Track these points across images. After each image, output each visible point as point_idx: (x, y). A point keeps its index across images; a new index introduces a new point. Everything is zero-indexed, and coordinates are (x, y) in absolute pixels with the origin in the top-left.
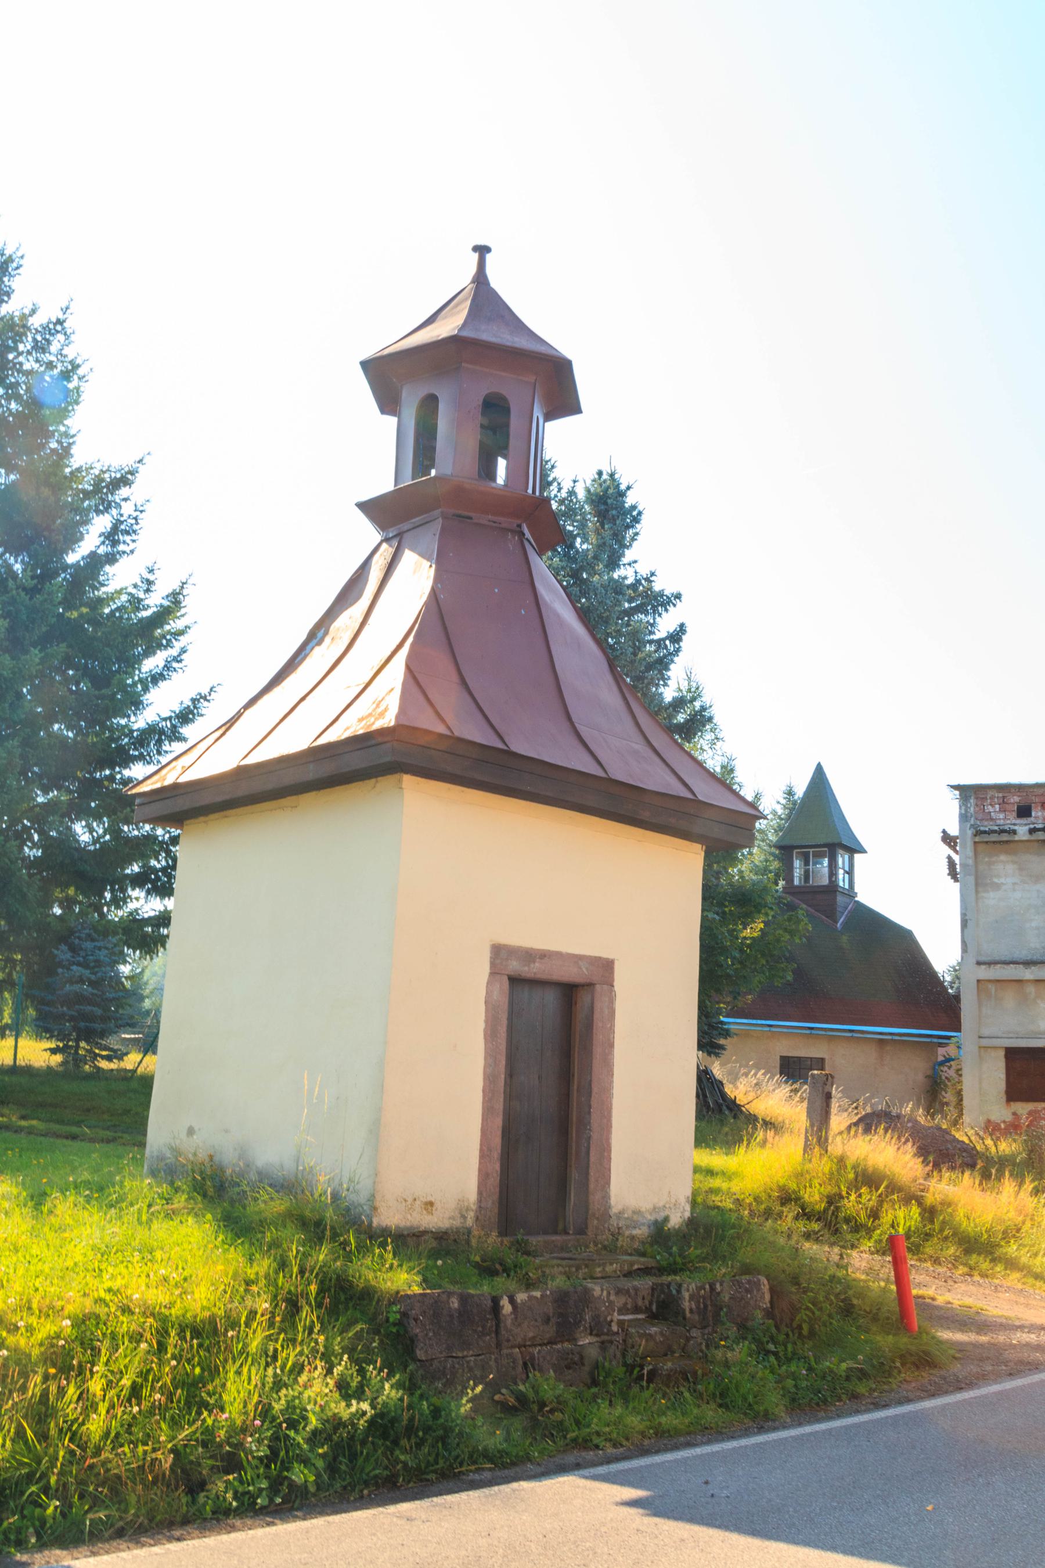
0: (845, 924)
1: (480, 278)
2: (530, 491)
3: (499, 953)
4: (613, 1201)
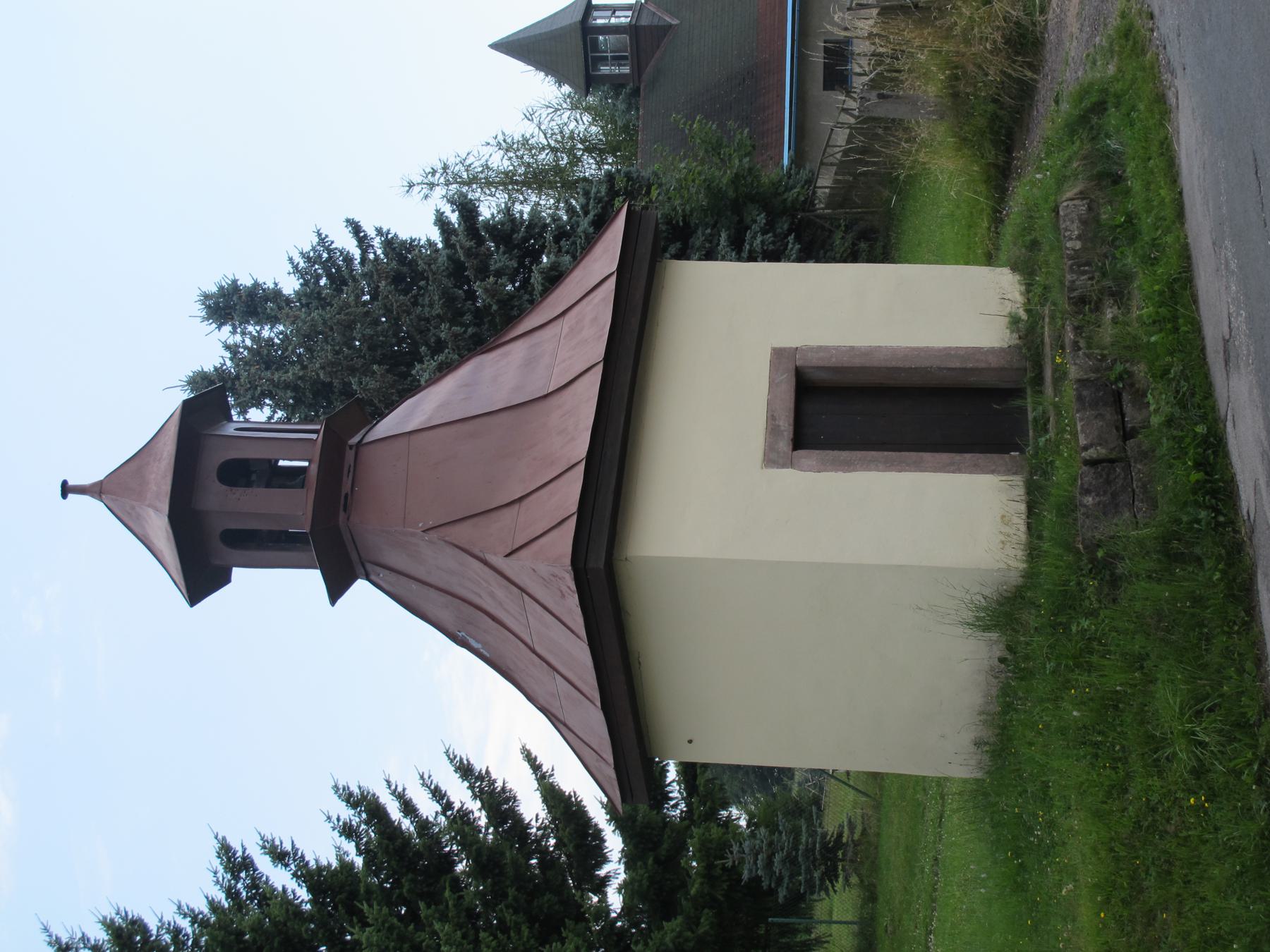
0: (672, 14)
1: (96, 490)
2: (314, 436)
3: (771, 459)
4: (996, 344)
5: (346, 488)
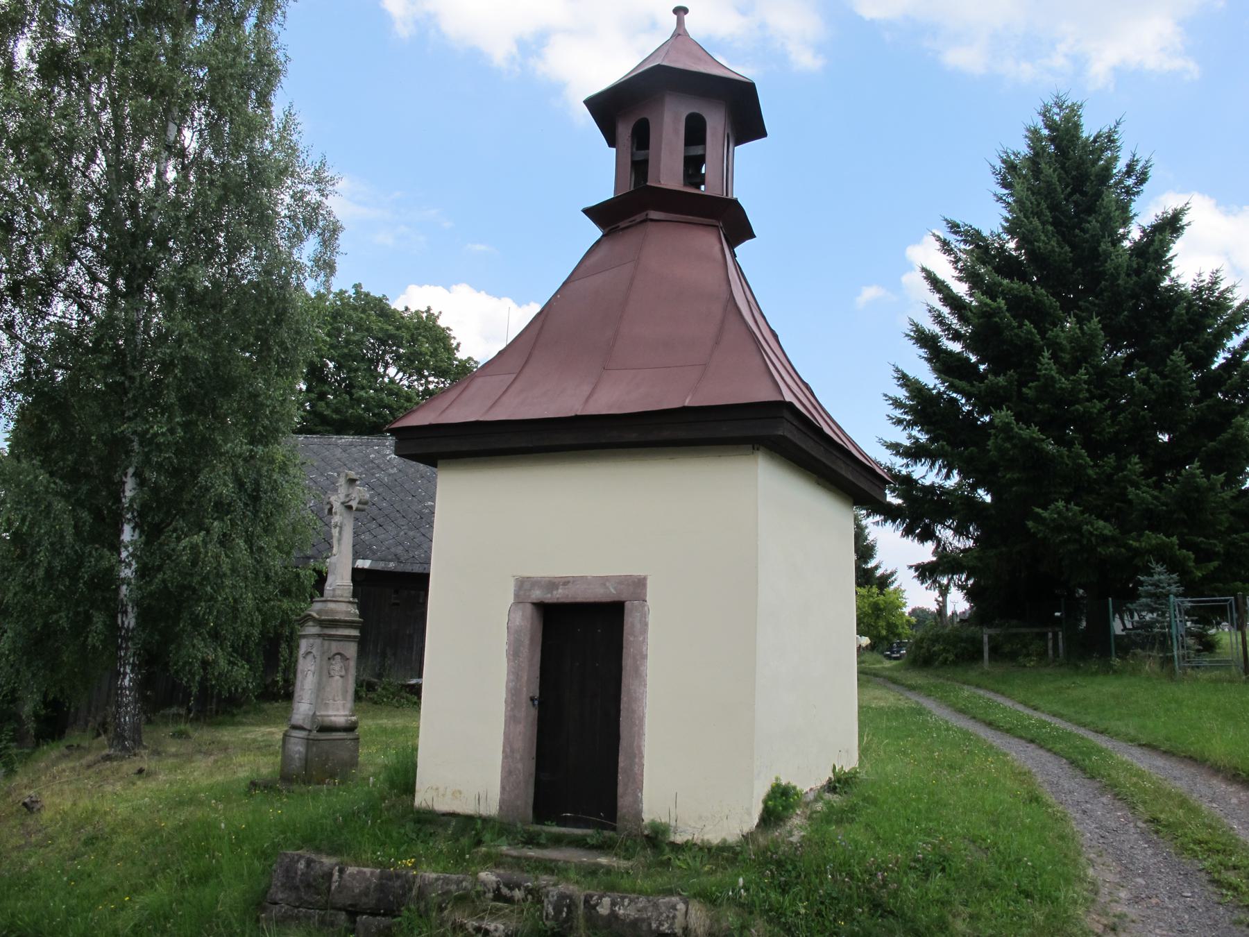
3: (639, 584)
4: (646, 806)
5: (622, 225)
